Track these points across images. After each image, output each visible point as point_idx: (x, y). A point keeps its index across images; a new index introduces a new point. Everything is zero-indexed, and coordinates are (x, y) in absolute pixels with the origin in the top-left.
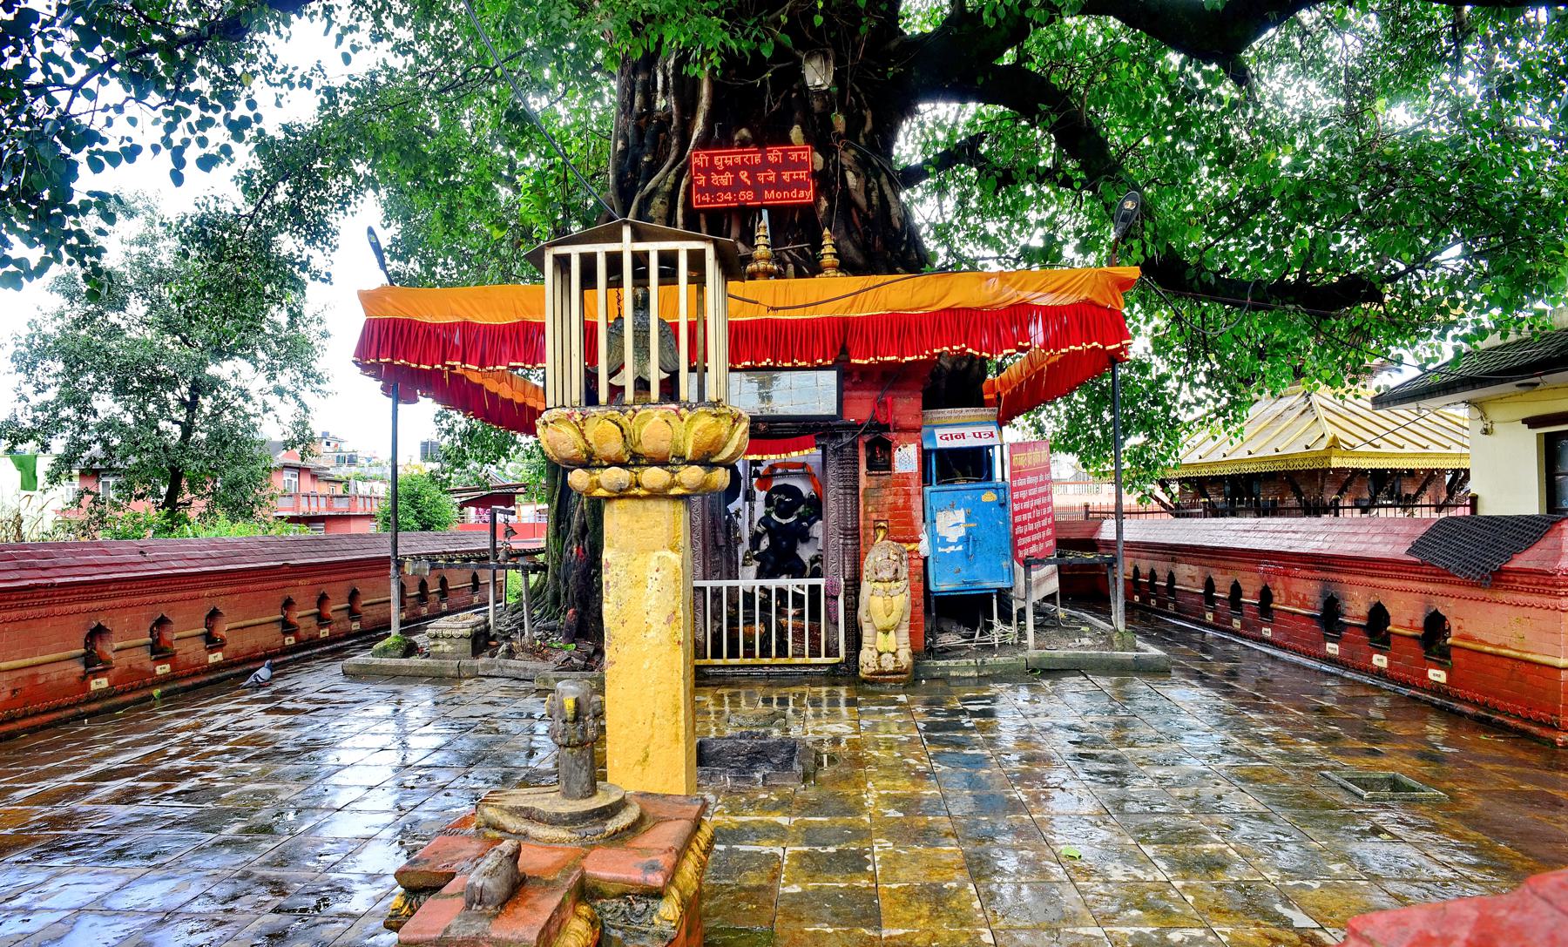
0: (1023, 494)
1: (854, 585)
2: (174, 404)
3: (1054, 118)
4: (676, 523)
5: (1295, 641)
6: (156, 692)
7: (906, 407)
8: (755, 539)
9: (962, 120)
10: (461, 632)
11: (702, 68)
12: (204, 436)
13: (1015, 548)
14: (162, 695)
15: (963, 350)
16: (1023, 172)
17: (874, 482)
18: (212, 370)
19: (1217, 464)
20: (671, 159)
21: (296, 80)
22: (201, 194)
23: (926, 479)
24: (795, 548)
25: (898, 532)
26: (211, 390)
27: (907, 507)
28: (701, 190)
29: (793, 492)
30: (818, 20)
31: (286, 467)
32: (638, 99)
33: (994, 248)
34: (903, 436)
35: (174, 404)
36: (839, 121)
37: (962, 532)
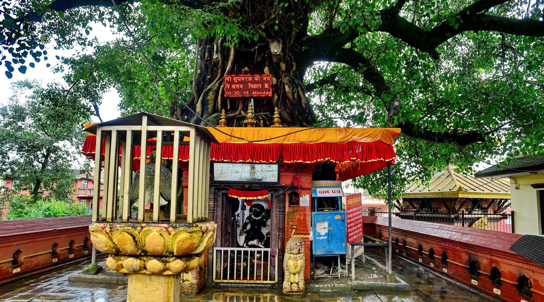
0: (351, 216)
1: (282, 251)
2: (40, 156)
3: (365, 69)
4: (169, 289)
5: (458, 276)
7: (305, 180)
8: (245, 225)
9: (329, 68)
11: (231, 44)
12: (50, 168)
13: (348, 237)
15: (329, 160)
16: (352, 88)
17: (291, 209)
18: (55, 144)
19: (417, 194)
20: (218, 77)
21: (87, 43)
22: (50, 82)
23: (313, 209)
24: (260, 229)
25: (301, 230)
26: (55, 151)
27: (305, 220)
28: (228, 90)
29: (261, 207)
30: (276, 28)
31: (82, 179)
32: (207, 54)
33: (347, 121)
34: (304, 191)
35: (40, 156)
36: (283, 66)
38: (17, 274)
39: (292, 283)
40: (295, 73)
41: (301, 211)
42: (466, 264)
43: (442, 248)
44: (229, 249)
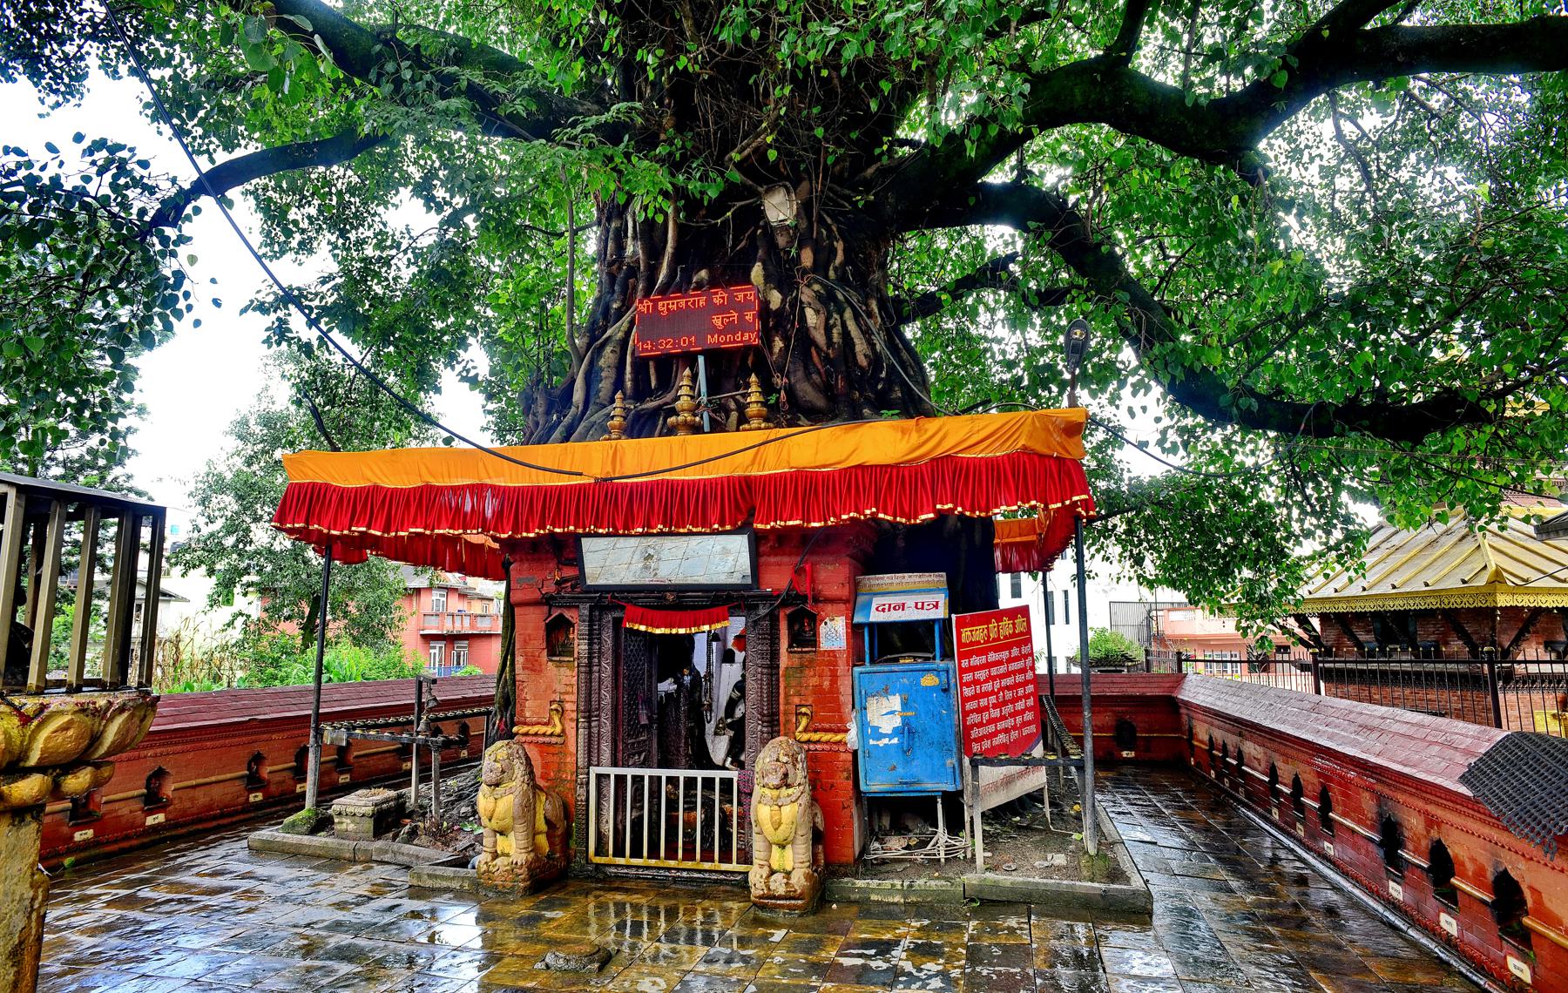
6: (67, 861)
7: (832, 576)
10: (363, 810)
14: (74, 865)
17: (796, 660)
19: (1385, 596)
34: (829, 607)
38: (156, 828)
40: (841, 271)
41: (821, 664)
42: (1371, 828)
43: (1319, 775)
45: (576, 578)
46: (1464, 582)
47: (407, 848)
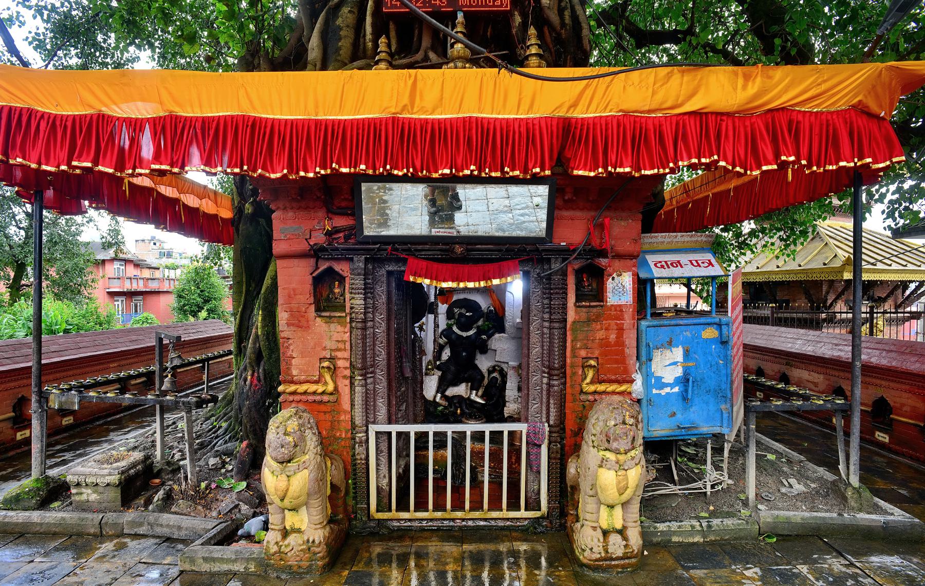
10: (108, 479)
17: (583, 313)
27: (620, 342)
29: (472, 306)
34: (617, 263)
37: (679, 372)
39: (605, 533)
41: (610, 318)
44: (413, 429)
45: (351, 228)
46: (825, 264)
47: (166, 518)
